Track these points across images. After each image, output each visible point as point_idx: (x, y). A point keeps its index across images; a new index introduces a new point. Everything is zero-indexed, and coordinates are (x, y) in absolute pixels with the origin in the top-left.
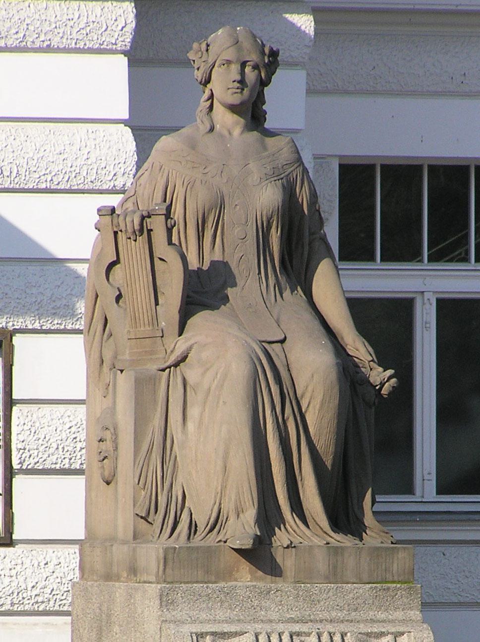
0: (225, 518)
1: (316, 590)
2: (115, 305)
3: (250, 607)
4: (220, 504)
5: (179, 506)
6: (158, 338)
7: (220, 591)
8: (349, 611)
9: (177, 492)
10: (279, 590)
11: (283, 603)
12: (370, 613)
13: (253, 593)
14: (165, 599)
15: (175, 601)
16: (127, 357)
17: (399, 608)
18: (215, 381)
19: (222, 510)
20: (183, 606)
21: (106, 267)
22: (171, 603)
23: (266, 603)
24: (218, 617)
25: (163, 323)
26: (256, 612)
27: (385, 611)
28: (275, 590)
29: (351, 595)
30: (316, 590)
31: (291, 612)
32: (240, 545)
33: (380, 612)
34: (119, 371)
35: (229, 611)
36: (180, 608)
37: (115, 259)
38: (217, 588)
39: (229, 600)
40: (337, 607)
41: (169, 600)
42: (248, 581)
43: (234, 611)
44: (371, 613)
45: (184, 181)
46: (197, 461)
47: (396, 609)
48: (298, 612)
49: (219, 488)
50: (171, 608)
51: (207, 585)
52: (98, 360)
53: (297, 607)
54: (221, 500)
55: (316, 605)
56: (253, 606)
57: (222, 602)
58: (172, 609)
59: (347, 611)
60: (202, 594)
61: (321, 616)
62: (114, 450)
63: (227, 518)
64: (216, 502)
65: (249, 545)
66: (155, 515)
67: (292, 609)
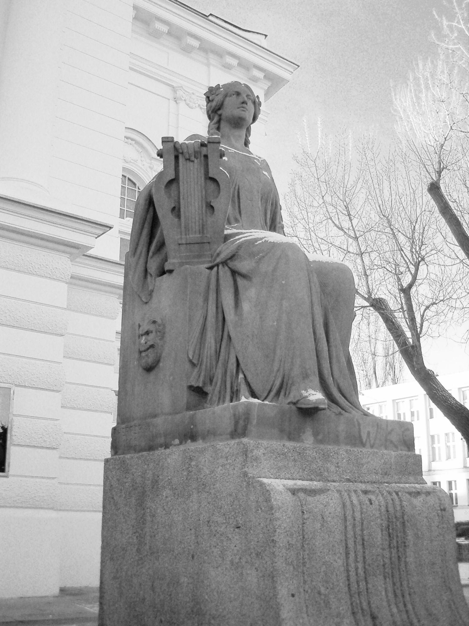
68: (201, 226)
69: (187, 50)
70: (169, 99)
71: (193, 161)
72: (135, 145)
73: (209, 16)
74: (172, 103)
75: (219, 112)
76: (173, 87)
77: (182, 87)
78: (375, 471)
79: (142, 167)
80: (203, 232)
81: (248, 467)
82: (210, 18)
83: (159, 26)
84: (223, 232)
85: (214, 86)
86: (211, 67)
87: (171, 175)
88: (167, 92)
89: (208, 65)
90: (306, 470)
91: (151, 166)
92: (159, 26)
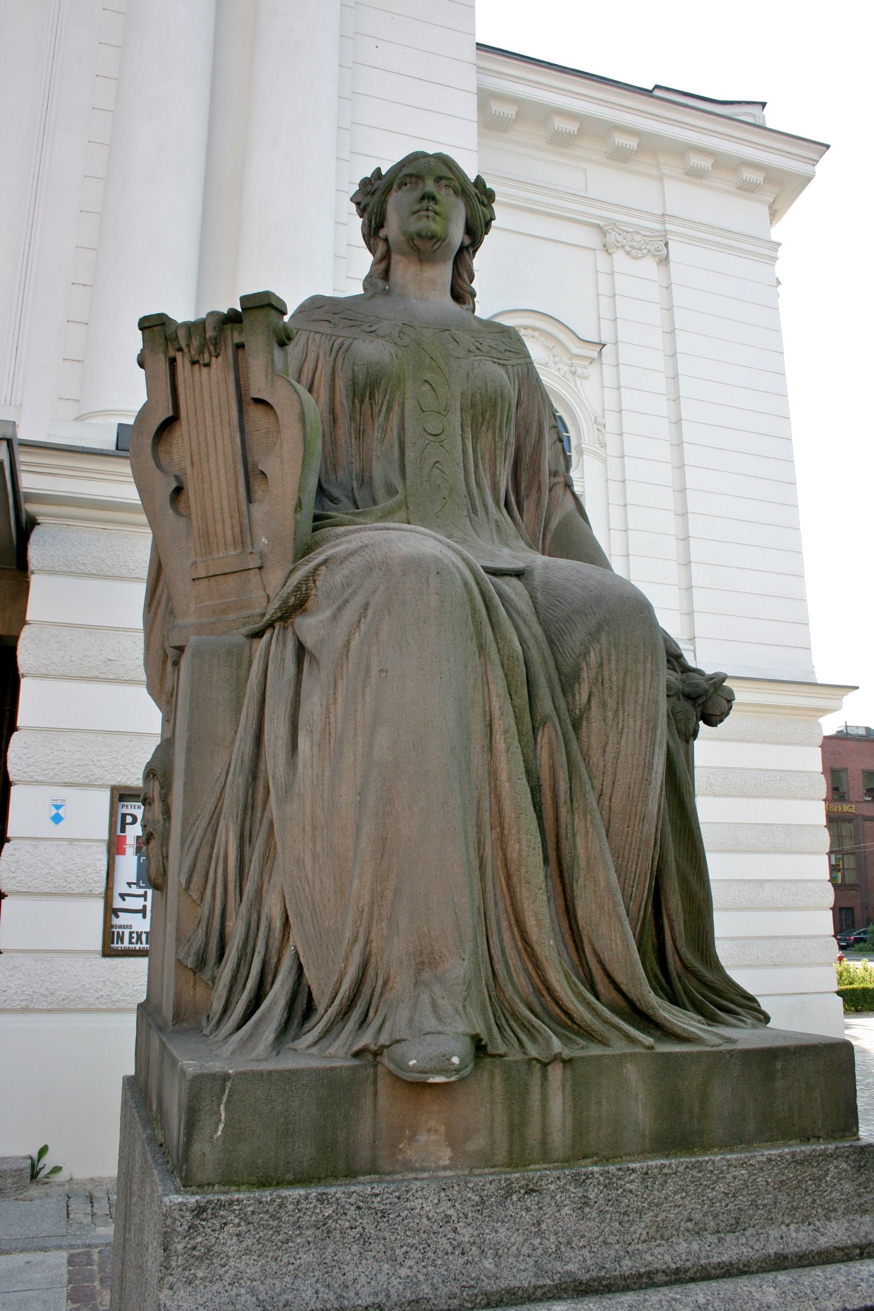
0: (380, 983)
1: (632, 1182)
2: (170, 512)
3: (450, 1249)
4: (367, 942)
5: (275, 943)
6: (253, 572)
7: (359, 1208)
8: (718, 1232)
9: (272, 908)
10: (533, 1191)
11: (544, 1226)
12: (770, 1232)
13: (458, 1206)
14: (180, 1247)
15: (217, 1248)
16: (191, 619)
17: (835, 1210)
18: (362, 625)
19: (373, 959)
20: (242, 1266)
21: (152, 436)
22: (200, 1258)
23: (497, 1232)
24: (352, 1294)
25: (264, 540)
26: (468, 1262)
27: (803, 1222)
28: (522, 1191)
29: (721, 1187)
30: (632, 1182)
31: (568, 1253)
32: (493, 542)
33: (792, 1227)
34: (538, 1066)
35: (386, 1266)
36: (232, 1272)
37: (171, 414)
38: (352, 1200)
39: (387, 1234)
40: (689, 1224)
41: (194, 1248)
42: (445, 1168)
43: (401, 1265)
44: (774, 1232)
45: (333, 345)
46: (314, 828)
47: (829, 1213)
48: (585, 1252)
49: (367, 896)
50: (200, 1274)
51: (321, 1190)
52: (160, 653)
53: (583, 1236)
54: (370, 932)
55: (632, 1222)
56: (459, 1244)
57: (364, 1239)
58: (203, 1279)
59: (713, 1234)
60: (304, 1222)
61: (649, 1258)
62: (164, 819)
63: (385, 983)
64: (357, 936)
65: (415, 549)
66: (218, 967)
67: (569, 1243)
68: (237, 529)
69: (695, 175)
70: (595, 250)
71: (208, 365)
72: (541, 339)
73: (654, 89)
74: (601, 256)
75: (382, 233)
76: (599, 227)
77: (614, 224)
78: (690, 1225)
79: (557, 374)
80: (243, 544)
81: (171, 1288)
82: (657, 93)
83: (621, 140)
84: (267, 544)
85: (369, 176)
86: (665, 180)
87: (164, 412)
88: (587, 237)
89: (661, 178)
90: (410, 1263)
91: (572, 369)
92: (621, 140)
